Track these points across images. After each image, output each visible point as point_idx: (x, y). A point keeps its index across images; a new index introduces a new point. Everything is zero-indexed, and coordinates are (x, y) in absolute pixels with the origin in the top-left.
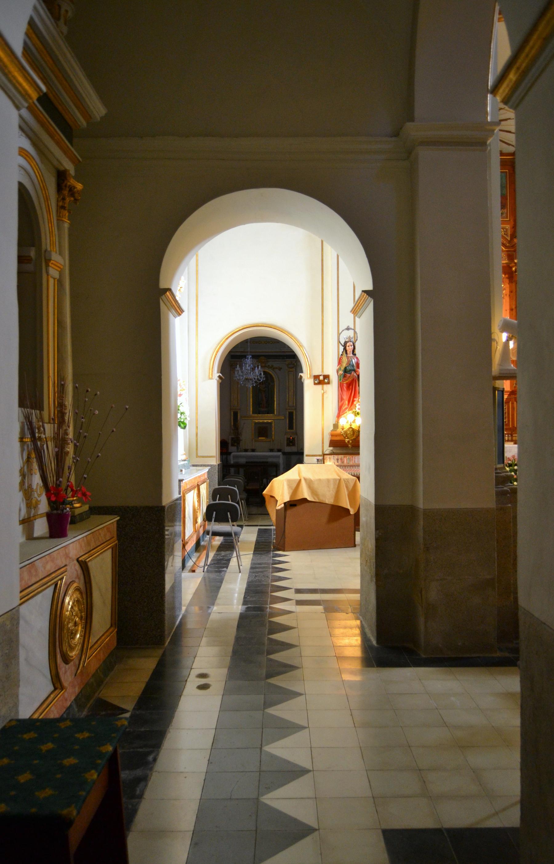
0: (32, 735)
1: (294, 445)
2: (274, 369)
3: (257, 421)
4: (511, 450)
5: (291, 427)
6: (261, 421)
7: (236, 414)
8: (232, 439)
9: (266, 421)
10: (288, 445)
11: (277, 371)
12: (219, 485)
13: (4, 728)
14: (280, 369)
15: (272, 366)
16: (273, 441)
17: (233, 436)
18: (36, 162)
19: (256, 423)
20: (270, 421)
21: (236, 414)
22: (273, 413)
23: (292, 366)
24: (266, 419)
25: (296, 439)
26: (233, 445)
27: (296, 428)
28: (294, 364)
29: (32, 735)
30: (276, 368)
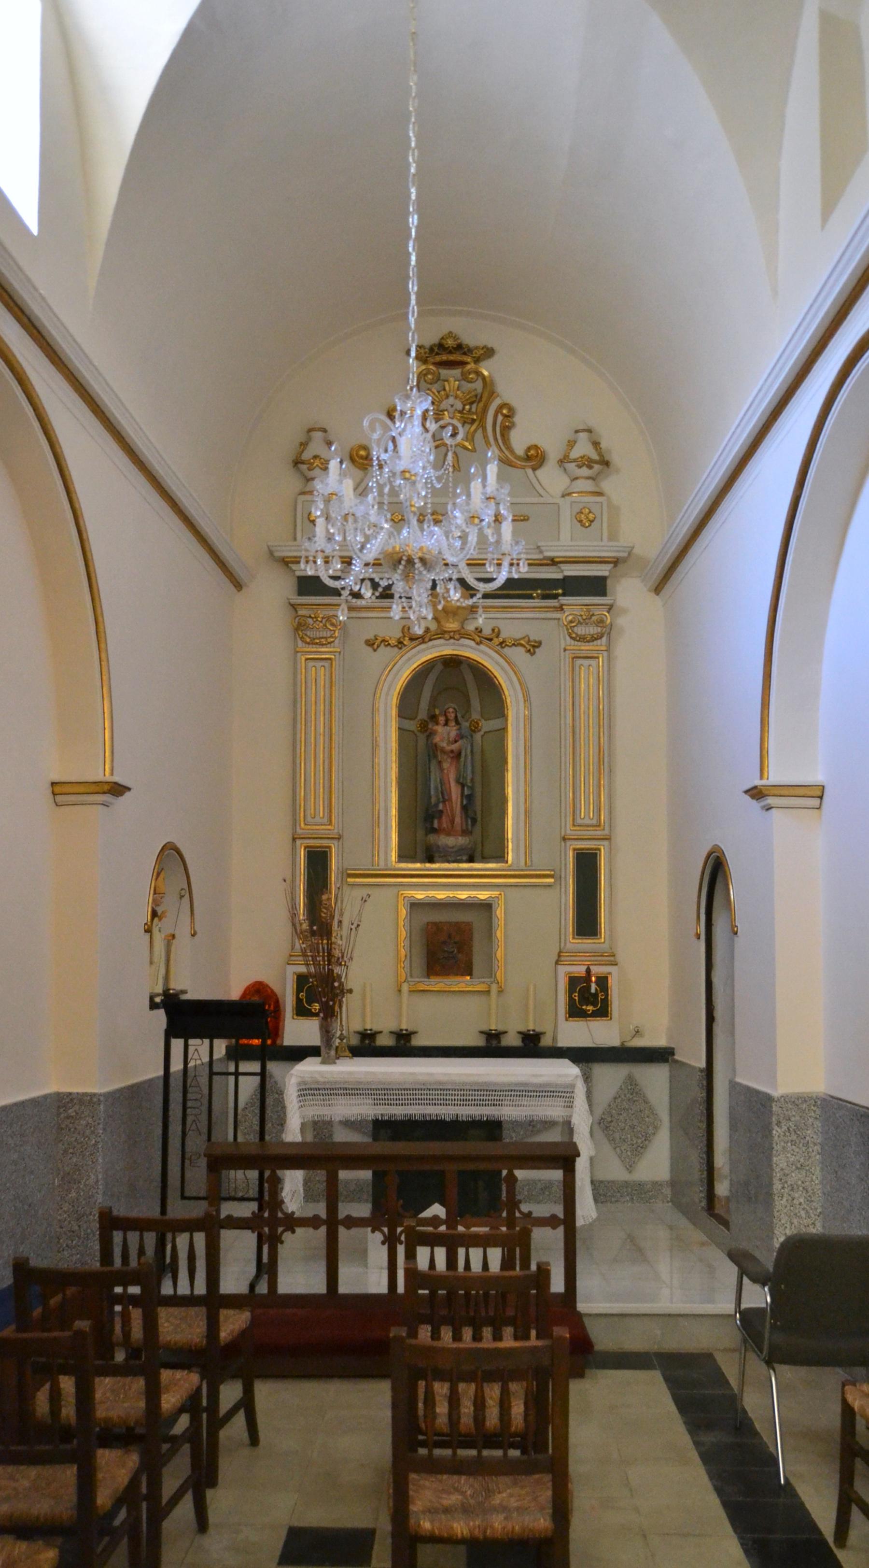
0: (123, 1514)
1: (603, 1012)
2: (502, 644)
3: (420, 895)
4: (315, 928)
5: (587, 921)
6: (441, 895)
7: (318, 861)
8: (301, 980)
9: (463, 895)
10: (575, 1012)
11: (518, 654)
12: (102, 1265)
13: (3, 1565)
14: (533, 647)
15: (496, 632)
16: (501, 991)
17: (303, 969)
18: (386, 699)
19: (415, 906)
20: (483, 895)
21: (318, 861)
22: (500, 856)
23: (593, 630)
24: (452, 885)
25: (613, 983)
26: (302, 1011)
27: (611, 930)
28: (601, 622)
29: (123, 1514)
30: (516, 644)
